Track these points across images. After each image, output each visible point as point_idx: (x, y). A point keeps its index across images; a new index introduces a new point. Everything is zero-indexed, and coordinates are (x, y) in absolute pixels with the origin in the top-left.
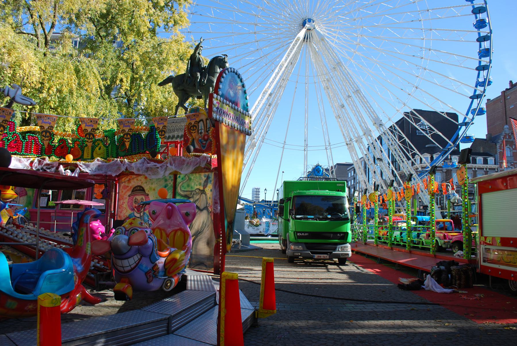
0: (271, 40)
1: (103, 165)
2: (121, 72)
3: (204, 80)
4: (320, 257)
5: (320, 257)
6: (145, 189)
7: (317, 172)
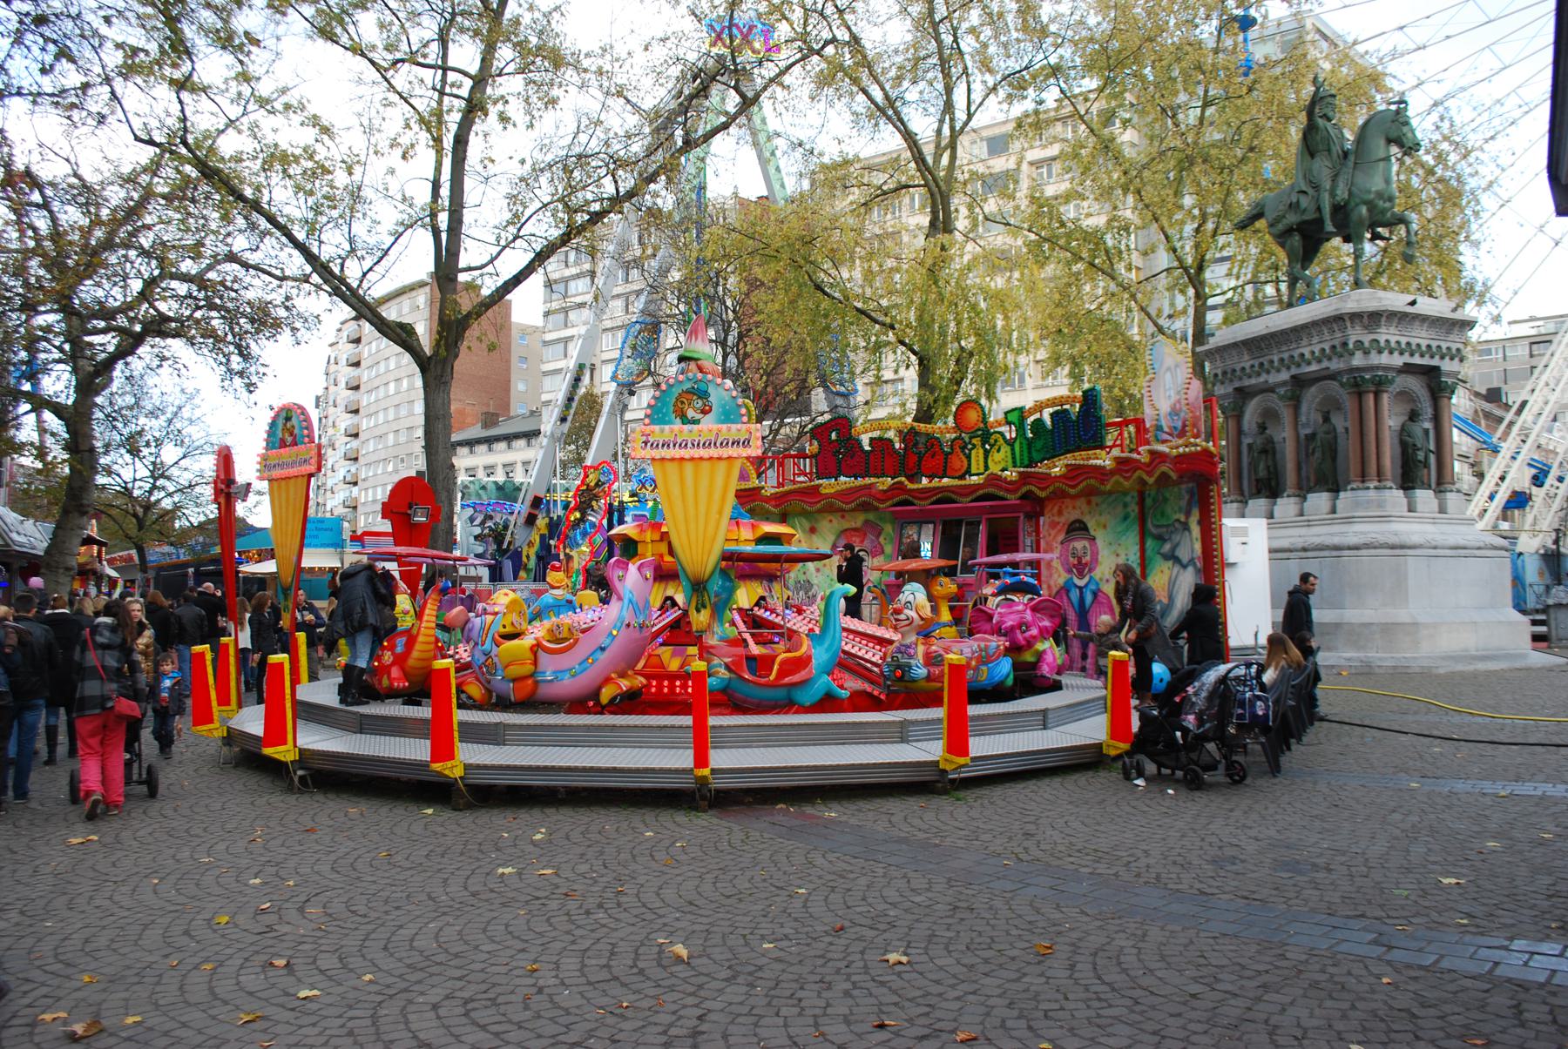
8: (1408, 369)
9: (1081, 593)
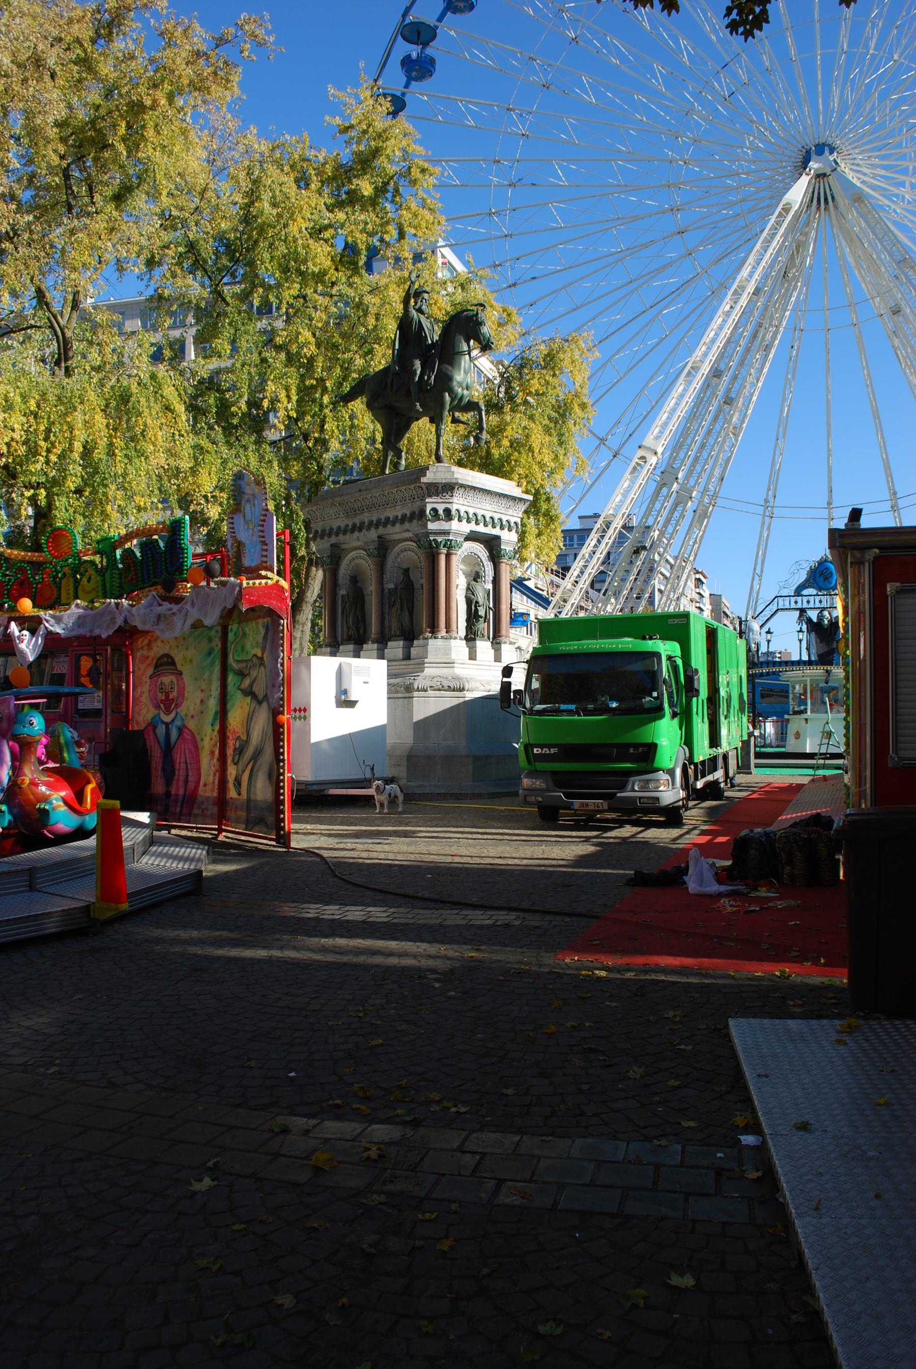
0: (718, 222)
1: (88, 616)
2: (272, 377)
3: (429, 378)
4: (587, 805)
5: (587, 805)
6: (176, 660)
7: (822, 578)
8: (472, 537)
9: (167, 729)
